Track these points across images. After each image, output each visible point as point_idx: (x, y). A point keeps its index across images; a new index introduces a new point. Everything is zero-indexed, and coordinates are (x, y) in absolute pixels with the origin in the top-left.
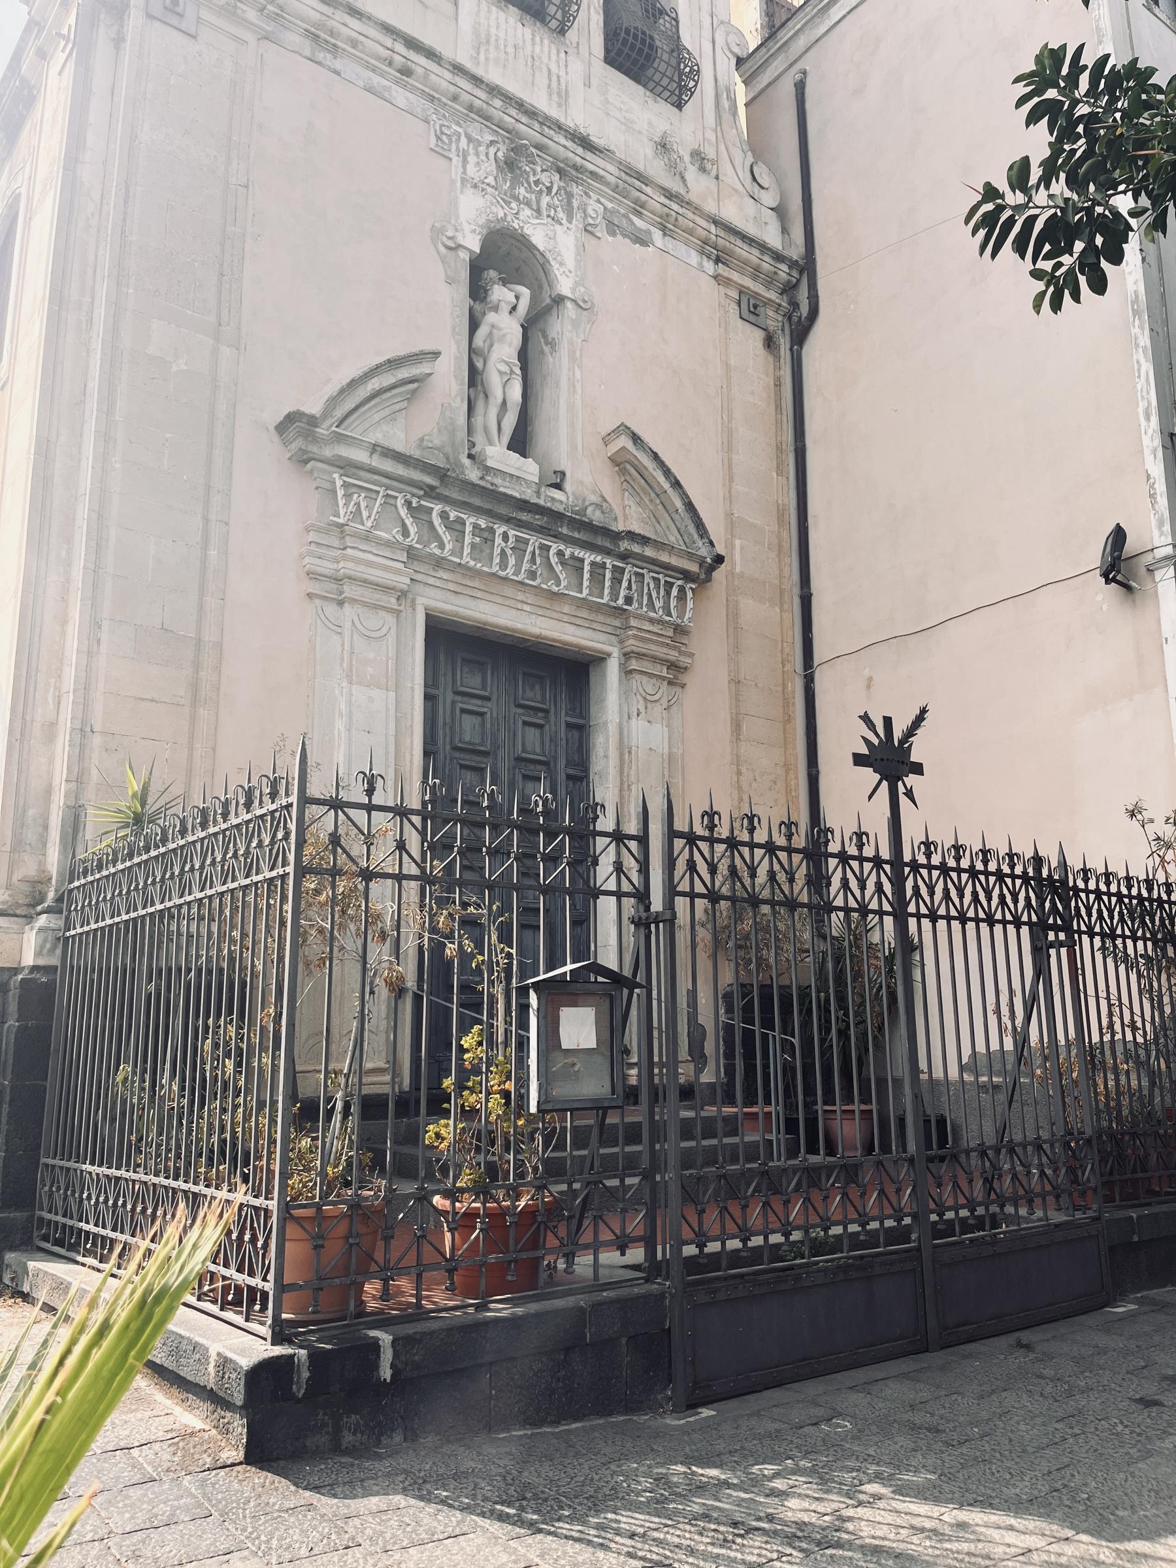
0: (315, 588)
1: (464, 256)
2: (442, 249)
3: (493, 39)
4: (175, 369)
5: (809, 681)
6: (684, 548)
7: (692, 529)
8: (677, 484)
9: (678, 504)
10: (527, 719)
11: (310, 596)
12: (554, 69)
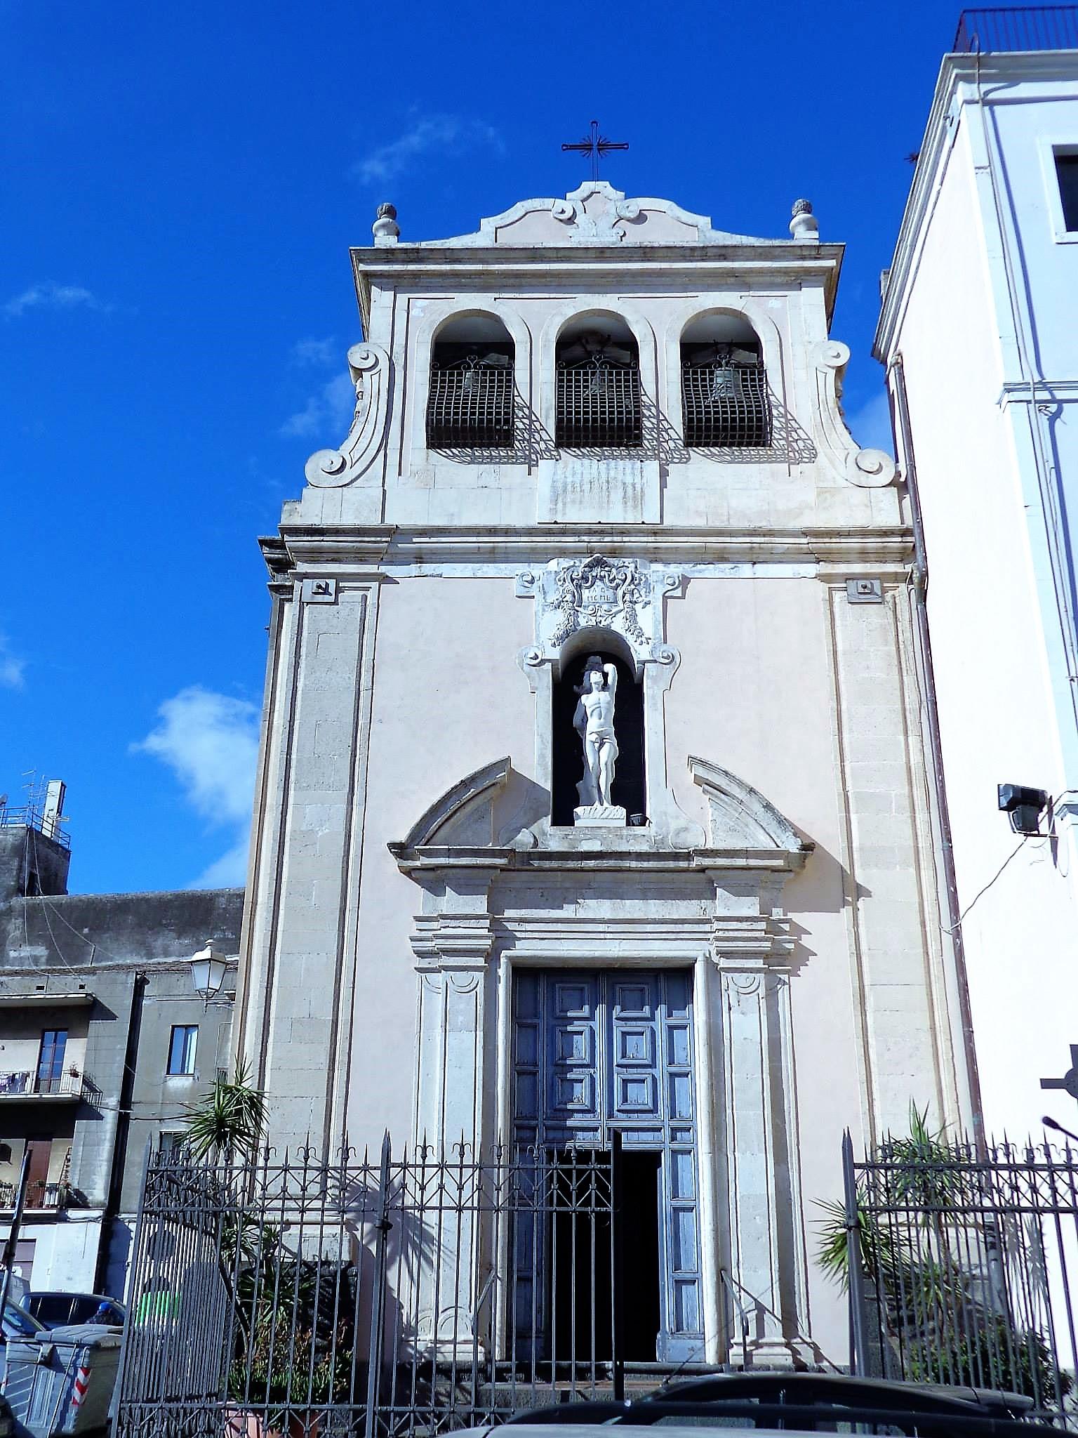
0: (425, 963)
1: (548, 666)
2: (526, 668)
3: (569, 487)
4: (320, 834)
5: (957, 934)
6: (773, 846)
7: (773, 827)
8: (752, 791)
9: (757, 808)
10: (625, 1029)
11: (419, 970)
12: (629, 480)
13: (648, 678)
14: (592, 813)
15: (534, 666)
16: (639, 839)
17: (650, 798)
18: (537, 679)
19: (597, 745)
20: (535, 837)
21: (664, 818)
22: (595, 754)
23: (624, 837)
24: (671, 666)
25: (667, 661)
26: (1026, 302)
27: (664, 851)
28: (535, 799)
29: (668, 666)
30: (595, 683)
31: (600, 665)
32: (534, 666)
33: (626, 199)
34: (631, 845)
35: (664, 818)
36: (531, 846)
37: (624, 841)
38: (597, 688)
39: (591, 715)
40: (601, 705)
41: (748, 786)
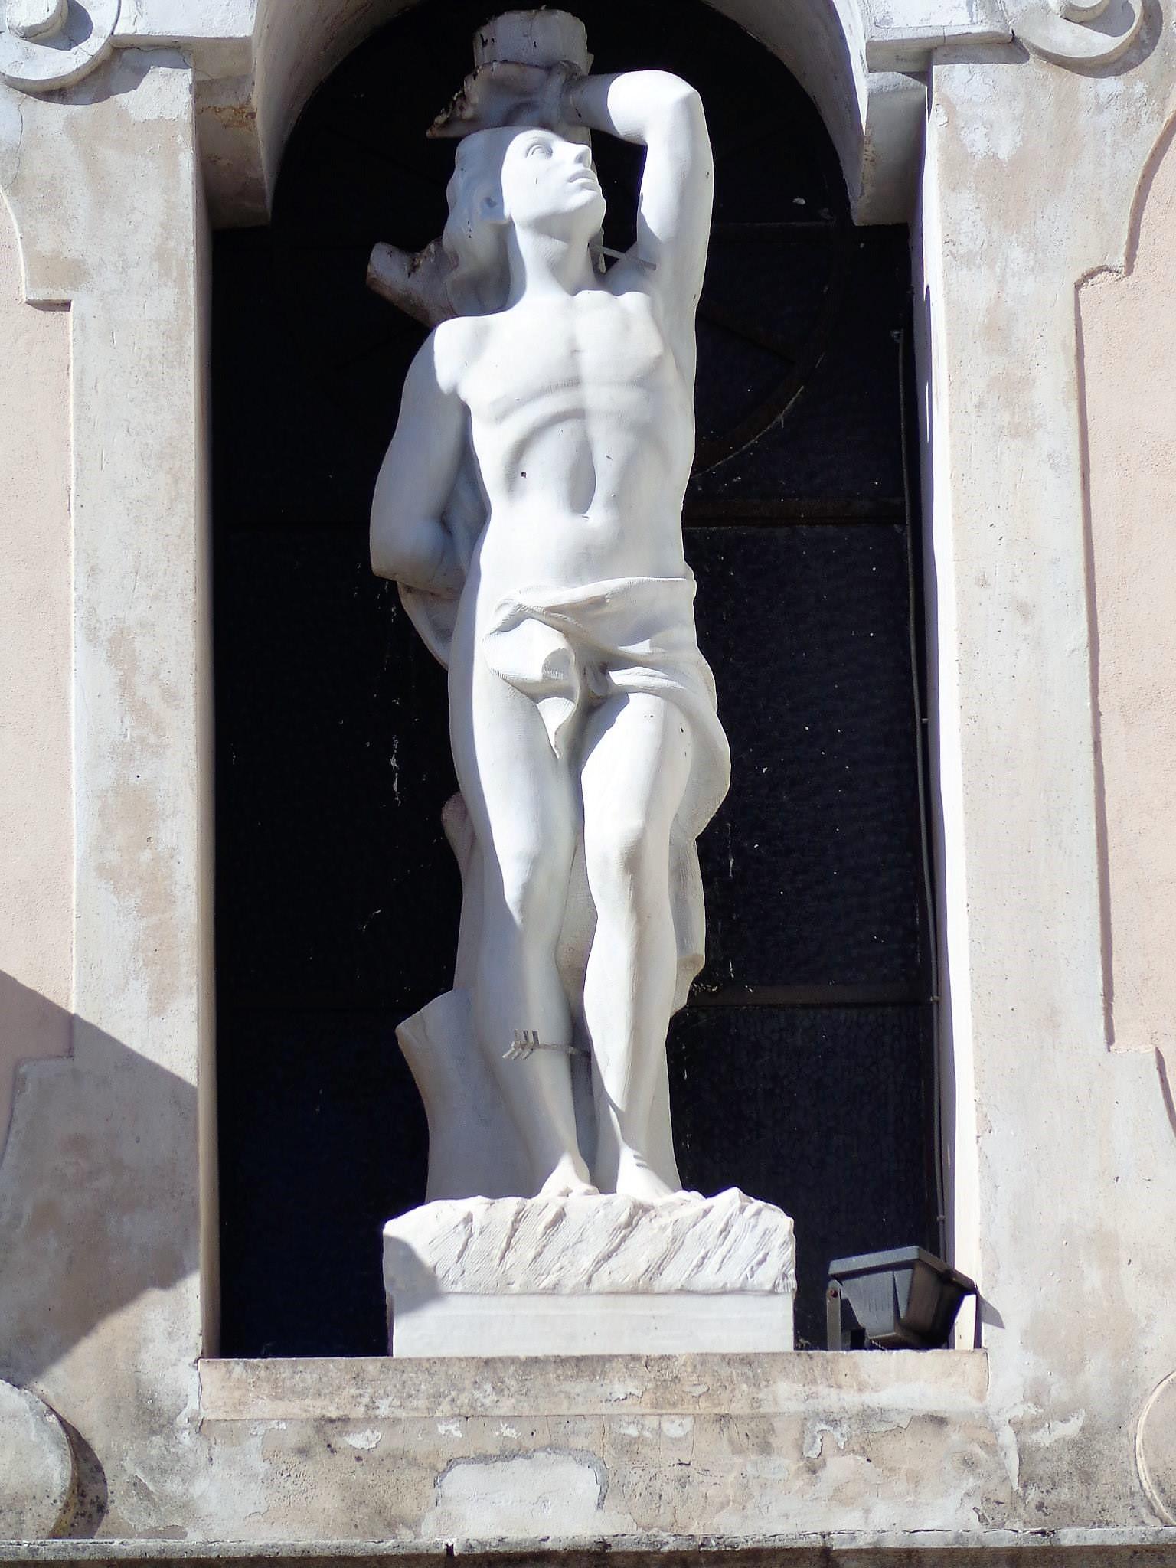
13: (952, 185)
14: (525, 1251)
15: (55, 92)
16: (905, 1451)
17: (986, 1127)
18: (79, 197)
19: (557, 714)
20: (79, 1446)
21: (1094, 1278)
22: (537, 776)
23: (784, 1438)
24: (1135, 83)
25: (1101, 43)
26: (1095, 850)
27: (1094, 1536)
28: (78, 1144)
29: (1110, 85)
30: (544, 225)
31: (573, 80)
32: (55, 92)
33: (617, 259)
34: (839, 1497)
35: (1094, 1278)
36: (50, 1513)
37: (784, 1463)
38: (556, 269)
39: (515, 471)
40: (598, 396)
41: (967, 1351)
